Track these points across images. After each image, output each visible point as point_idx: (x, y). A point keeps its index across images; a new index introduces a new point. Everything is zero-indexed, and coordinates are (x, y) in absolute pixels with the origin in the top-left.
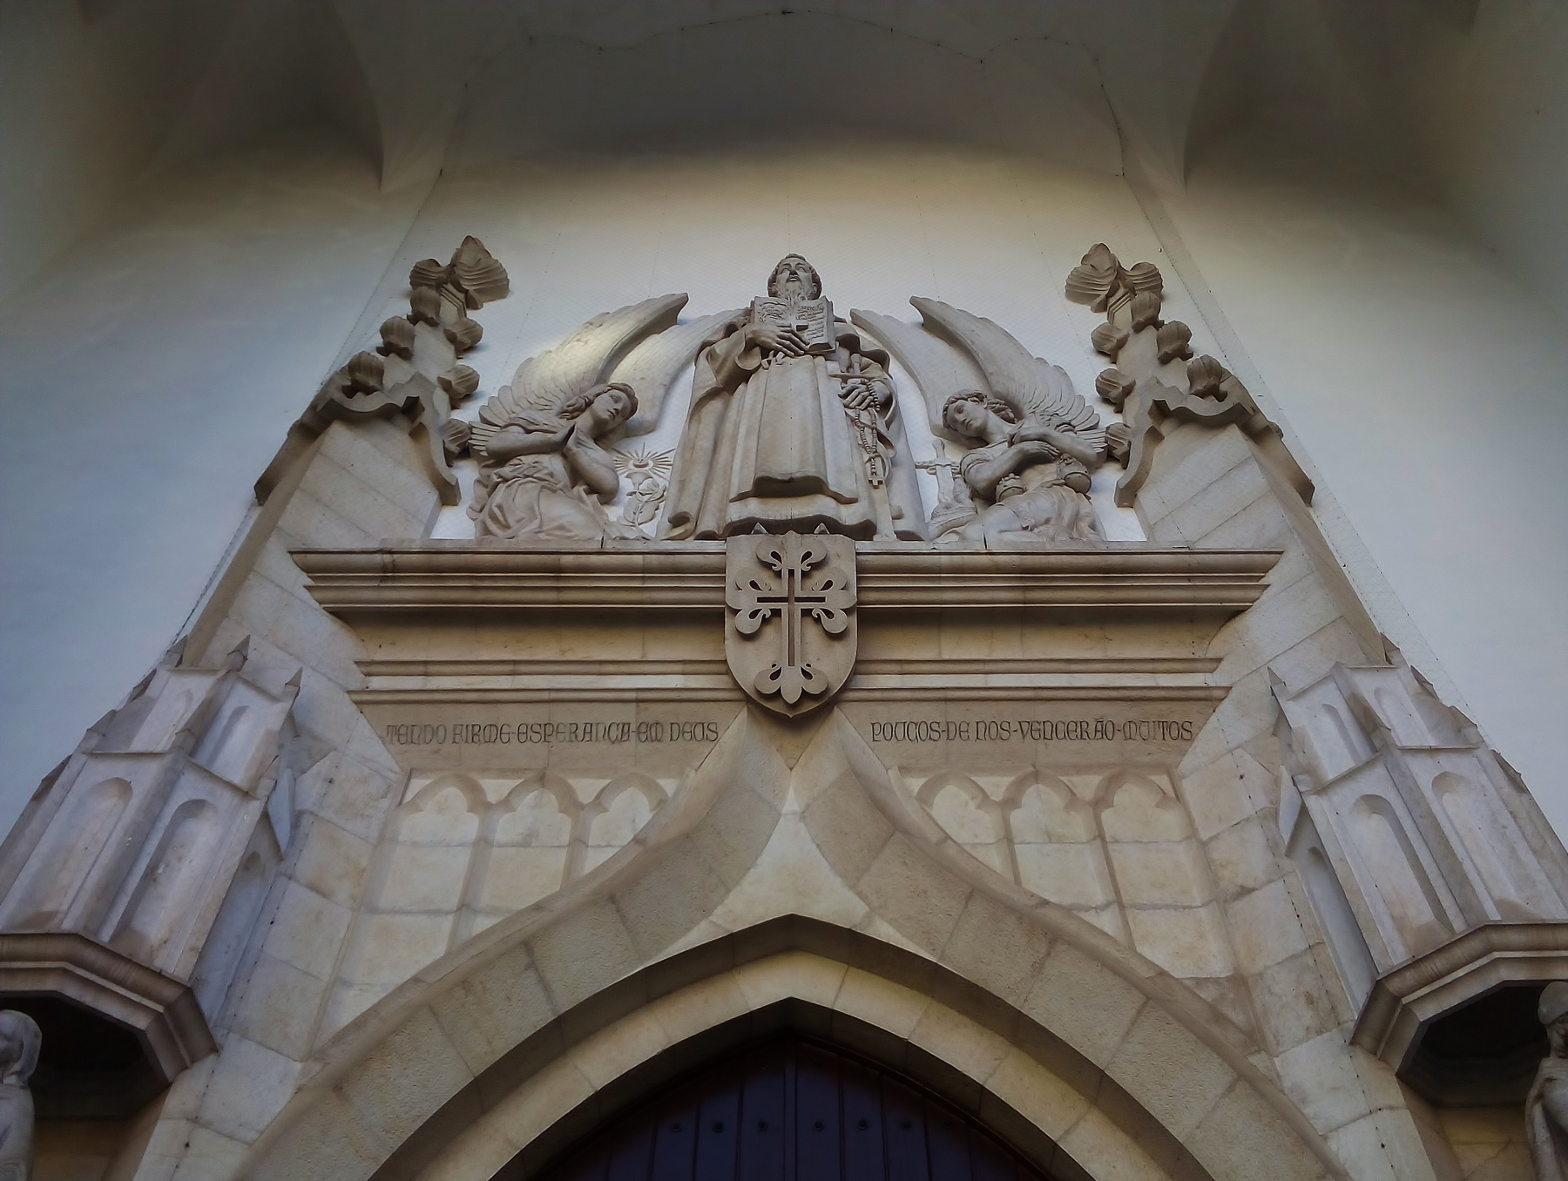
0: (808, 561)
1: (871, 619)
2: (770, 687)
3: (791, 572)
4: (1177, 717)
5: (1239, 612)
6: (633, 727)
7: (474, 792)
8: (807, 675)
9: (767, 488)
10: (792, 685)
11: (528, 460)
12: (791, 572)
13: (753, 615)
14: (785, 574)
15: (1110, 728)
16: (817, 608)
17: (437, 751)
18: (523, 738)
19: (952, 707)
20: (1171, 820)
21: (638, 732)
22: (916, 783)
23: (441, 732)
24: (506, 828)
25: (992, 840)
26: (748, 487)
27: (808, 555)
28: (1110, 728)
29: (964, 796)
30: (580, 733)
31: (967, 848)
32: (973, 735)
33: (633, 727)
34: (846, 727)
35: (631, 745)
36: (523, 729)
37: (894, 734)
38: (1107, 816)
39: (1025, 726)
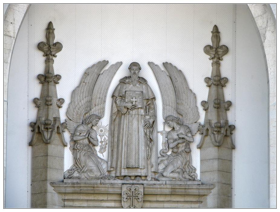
3: (133, 192)
12: (133, 192)
13: (127, 198)
14: (132, 192)
16: (137, 197)
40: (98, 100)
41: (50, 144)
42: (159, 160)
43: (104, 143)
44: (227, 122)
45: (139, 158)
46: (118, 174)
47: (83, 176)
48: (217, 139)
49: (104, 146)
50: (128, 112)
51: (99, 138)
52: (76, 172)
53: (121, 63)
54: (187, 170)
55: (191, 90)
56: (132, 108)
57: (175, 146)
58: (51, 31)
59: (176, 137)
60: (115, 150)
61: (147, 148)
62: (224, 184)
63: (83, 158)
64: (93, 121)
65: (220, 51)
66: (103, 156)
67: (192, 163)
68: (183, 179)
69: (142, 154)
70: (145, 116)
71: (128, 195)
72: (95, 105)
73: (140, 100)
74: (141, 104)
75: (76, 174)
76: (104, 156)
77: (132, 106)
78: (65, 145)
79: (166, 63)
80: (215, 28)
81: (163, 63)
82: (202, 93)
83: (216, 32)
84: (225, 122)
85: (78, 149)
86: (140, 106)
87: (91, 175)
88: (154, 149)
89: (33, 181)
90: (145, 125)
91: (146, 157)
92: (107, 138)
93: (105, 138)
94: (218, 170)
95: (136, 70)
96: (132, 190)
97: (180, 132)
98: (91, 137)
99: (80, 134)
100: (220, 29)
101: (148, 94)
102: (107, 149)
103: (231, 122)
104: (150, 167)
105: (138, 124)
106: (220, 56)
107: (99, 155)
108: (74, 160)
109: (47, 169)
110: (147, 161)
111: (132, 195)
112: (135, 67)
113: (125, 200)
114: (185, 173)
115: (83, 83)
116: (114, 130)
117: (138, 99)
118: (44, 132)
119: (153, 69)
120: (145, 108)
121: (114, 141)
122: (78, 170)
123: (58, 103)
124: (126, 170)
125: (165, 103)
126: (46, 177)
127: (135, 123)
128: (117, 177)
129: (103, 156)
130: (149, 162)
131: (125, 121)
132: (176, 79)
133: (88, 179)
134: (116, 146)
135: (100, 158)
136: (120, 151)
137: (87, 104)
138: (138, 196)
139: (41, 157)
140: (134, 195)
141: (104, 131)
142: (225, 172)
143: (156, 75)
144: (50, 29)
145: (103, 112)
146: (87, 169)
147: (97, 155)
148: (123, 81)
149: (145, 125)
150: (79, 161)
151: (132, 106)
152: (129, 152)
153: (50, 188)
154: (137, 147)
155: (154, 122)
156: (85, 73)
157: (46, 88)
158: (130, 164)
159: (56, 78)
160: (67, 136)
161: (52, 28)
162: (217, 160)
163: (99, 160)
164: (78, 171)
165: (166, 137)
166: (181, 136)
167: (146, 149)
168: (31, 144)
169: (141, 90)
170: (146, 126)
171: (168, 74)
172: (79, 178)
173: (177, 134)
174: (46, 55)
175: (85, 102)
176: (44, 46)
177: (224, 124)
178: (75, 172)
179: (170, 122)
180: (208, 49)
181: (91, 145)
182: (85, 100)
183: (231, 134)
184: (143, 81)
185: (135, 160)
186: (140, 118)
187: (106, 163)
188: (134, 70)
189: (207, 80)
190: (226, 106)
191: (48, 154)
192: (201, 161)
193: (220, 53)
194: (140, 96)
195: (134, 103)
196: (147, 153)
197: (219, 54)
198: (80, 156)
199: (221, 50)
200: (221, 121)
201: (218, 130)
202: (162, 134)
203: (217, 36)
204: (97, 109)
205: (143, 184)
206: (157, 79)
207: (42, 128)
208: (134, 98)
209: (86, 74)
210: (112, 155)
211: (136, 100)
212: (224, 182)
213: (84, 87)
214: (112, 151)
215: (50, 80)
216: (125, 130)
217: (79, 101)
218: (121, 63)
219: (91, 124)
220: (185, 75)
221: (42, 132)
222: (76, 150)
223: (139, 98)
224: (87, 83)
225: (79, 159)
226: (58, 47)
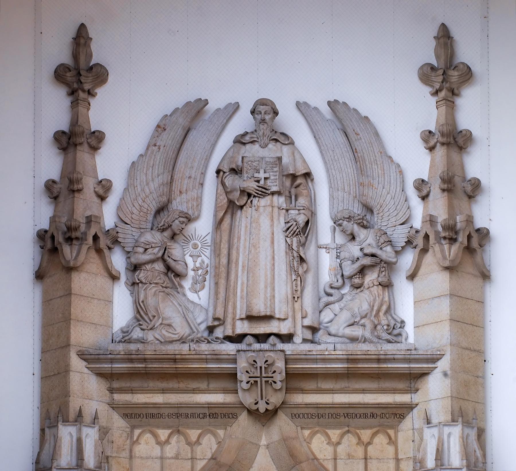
0: (267, 363)
1: (291, 376)
2: (254, 407)
3: (261, 367)
4: (400, 412)
5: (427, 374)
6: (208, 414)
7: (155, 436)
8: (268, 404)
9: (250, 318)
10: (262, 407)
11: (148, 267)
12: (261, 367)
13: (248, 383)
14: (259, 368)
15: (375, 415)
16: (270, 380)
17: (141, 421)
18: (170, 417)
19: (320, 409)
20: (391, 449)
21: (210, 416)
22: (307, 433)
23: (142, 415)
24: (170, 451)
25: (329, 458)
26: (244, 316)
27: (267, 361)
28: (375, 415)
29: (323, 439)
30: (189, 416)
31: (321, 461)
32: (327, 417)
33: (208, 414)
34: (283, 421)
35: (207, 419)
36: (169, 415)
37: (299, 416)
38: (370, 448)
39: (346, 415)
40: (186, 182)
41: (78, 271)
42: (322, 305)
43: (200, 272)
44: (470, 220)
45: (274, 296)
46: (229, 332)
47: (150, 336)
48: (447, 254)
49: (201, 277)
50: (249, 201)
51: (189, 261)
52: (138, 329)
53: (236, 107)
54: (384, 322)
55: (390, 157)
56: (258, 192)
57: (355, 272)
58: (82, 41)
59: (357, 253)
60: (222, 282)
61: (294, 277)
62: (467, 349)
63: (151, 301)
64: (173, 224)
65: (454, 75)
66: (200, 299)
67: (395, 308)
68: (375, 340)
69: (283, 288)
70: (287, 210)
71: (252, 375)
72: (180, 192)
73: (276, 175)
74: (277, 184)
75: (137, 333)
76: (201, 298)
77: (257, 188)
78: (114, 278)
79: (336, 101)
80: (441, 28)
81: (329, 103)
82: (418, 163)
83: (445, 37)
84: (465, 219)
85: (141, 282)
86: (274, 189)
87: (167, 334)
88: (310, 278)
89: (44, 351)
90: (288, 229)
91: (290, 297)
92: (207, 261)
93: (203, 262)
94: (450, 319)
95: (265, 113)
96: (259, 365)
97: (368, 242)
98: (169, 257)
99: (146, 250)
100: (455, 32)
101: (295, 166)
102: (207, 283)
103: (480, 223)
104: (299, 316)
105: (272, 226)
106: (454, 86)
107: (191, 296)
108: (135, 306)
109: (70, 323)
110: (293, 304)
111: (259, 375)
112: (265, 111)
113: (245, 386)
114: (379, 327)
115: (154, 148)
116: (221, 241)
117: (271, 173)
118: (63, 247)
119: (306, 115)
120: (287, 193)
121: (221, 263)
122: (140, 325)
123: (96, 190)
124: (246, 322)
125: (333, 185)
126: (68, 338)
127: (265, 222)
128: (230, 339)
129: (200, 299)
130: (297, 305)
131: (243, 219)
132: (357, 134)
133: (161, 342)
134: (224, 275)
135: (192, 302)
136: (232, 283)
137: (161, 190)
138: (272, 377)
139: (59, 299)
140: (264, 375)
141: (200, 246)
142: (467, 324)
143: (313, 128)
144: (81, 38)
145: (197, 206)
146: (160, 321)
147: (184, 295)
148: (240, 141)
149: (288, 229)
150: (143, 306)
151: (257, 188)
152: (250, 282)
153: (76, 363)
154: (269, 273)
155: (307, 223)
156: (158, 126)
157: (70, 156)
158: (255, 309)
159: (93, 138)
160: (118, 260)
161: (84, 35)
162: (448, 297)
163: (190, 306)
164: (142, 327)
165: (338, 257)
166: (367, 251)
167: (292, 278)
168: (39, 276)
169: (279, 155)
170: (290, 230)
171: (339, 126)
172: (142, 341)
173: (360, 247)
174: (72, 93)
175: (156, 185)
176: (66, 72)
177: (464, 224)
178: (134, 331)
179: (345, 223)
180: (426, 74)
181: (171, 274)
182: (157, 181)
183: (481, 246)
184: (282, 138)
185: (265, 301)
186: (277, 214)
187: (204, 311)
188: (261, 113)
189: (427, 136)
190: (469, 188)
191: (73, 292)
192: (415, 302)
193: (454, 79)
194: (276, 167)
195: (262, 182)
196: (292, 286)
197: (453, 80)
198: (146, 297)
199: (456, 73)
200: (458, 217)
201: (449, 235)
202: (328, 251)
203: (446, 44)
204: (185, 200)
205: (283, 351)
206: (316, 135)
207: (60, 238)
208: (262, 171)
209: (160, 128)
210: (217, 293)
211: (267, 175)
212: (464, 344)
213: (155, 156)
214: (217, 284)
215: (79, 140)
216: (242, 238)
217: (145, 183)
218: (236, 107)
219: (169, 229)
220: (375, 125)
221: (62, 248)
222: (138, 284)
223: (273, 172)
224: (162, 148)
225: (143, 302)
226: (100, 74)
